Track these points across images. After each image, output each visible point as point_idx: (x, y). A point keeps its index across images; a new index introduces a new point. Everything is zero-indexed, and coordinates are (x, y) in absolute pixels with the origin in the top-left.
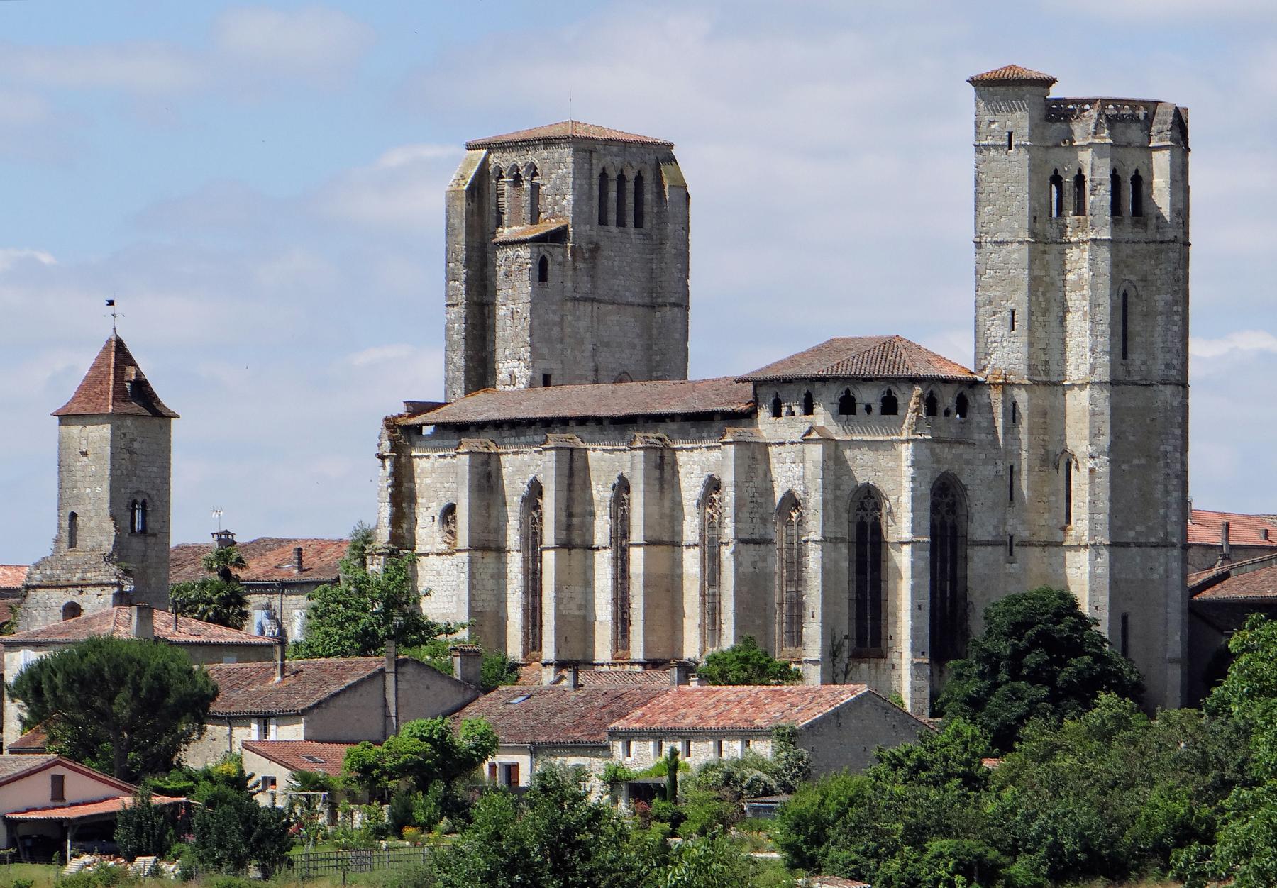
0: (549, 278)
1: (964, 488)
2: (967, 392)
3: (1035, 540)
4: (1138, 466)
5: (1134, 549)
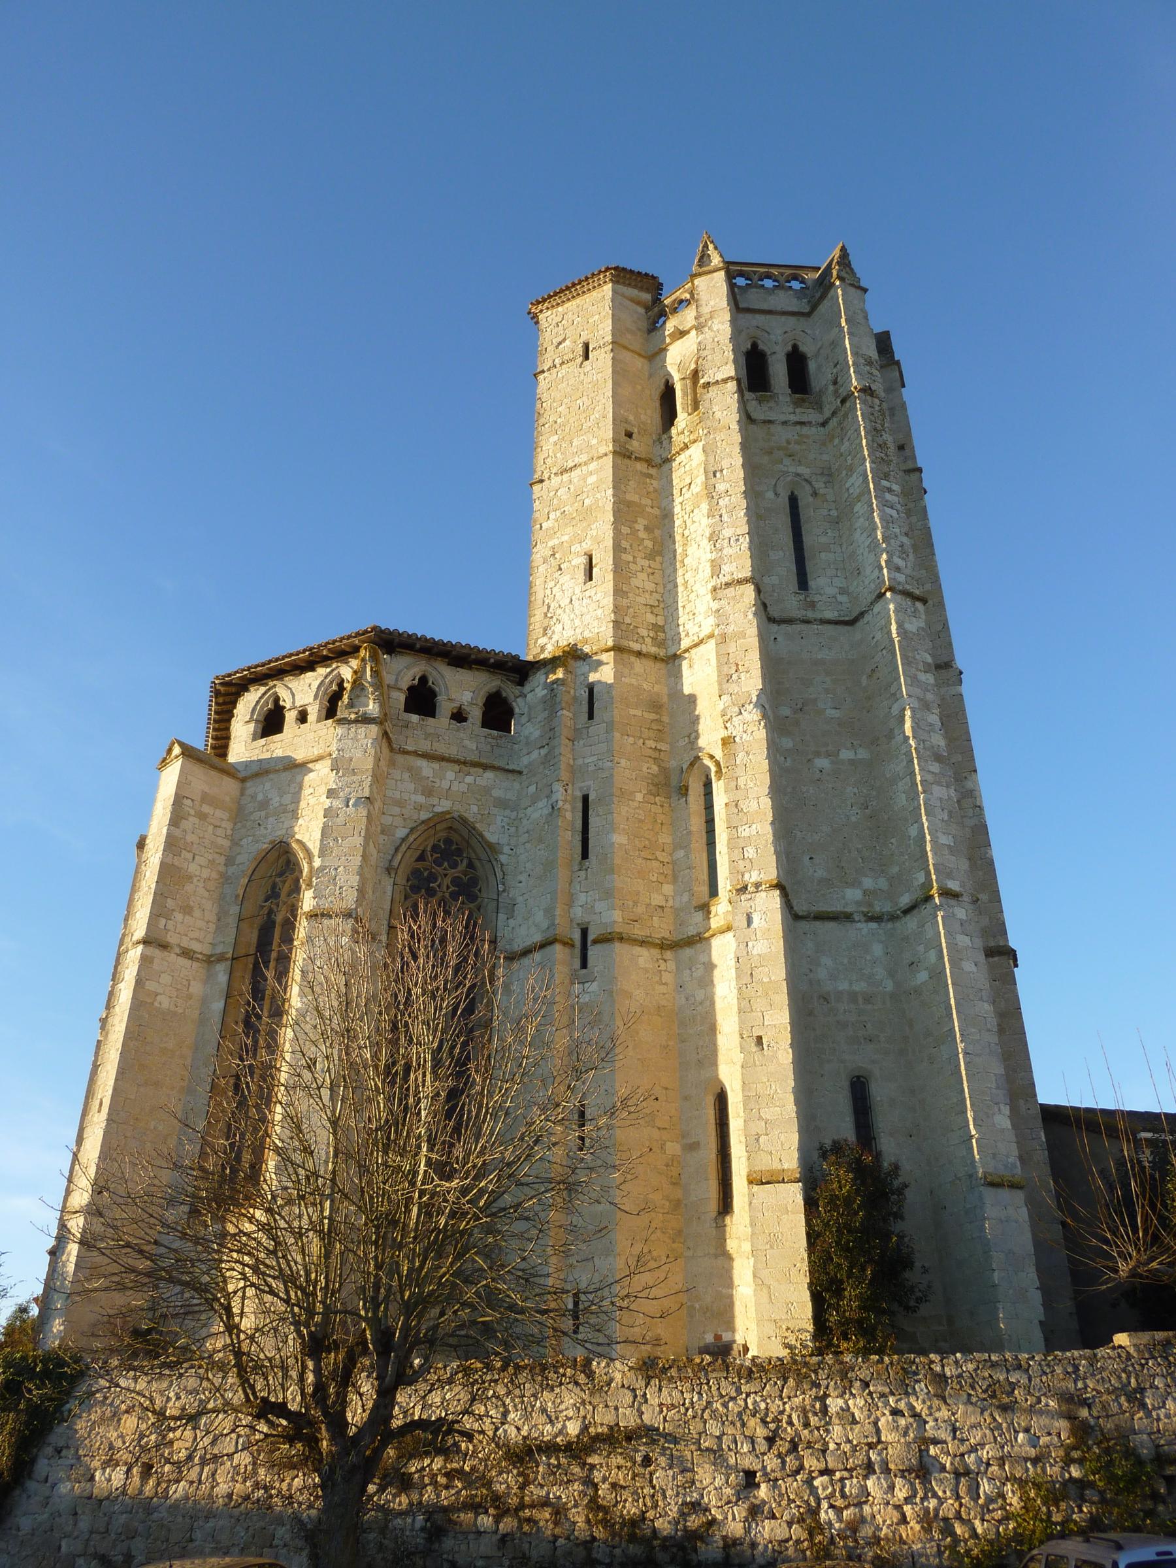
0: (846, 1084)
1: (493, 849)
2: (510, 691)
3: (638, 932)
4: (852, 762)
5: (866, 928)
